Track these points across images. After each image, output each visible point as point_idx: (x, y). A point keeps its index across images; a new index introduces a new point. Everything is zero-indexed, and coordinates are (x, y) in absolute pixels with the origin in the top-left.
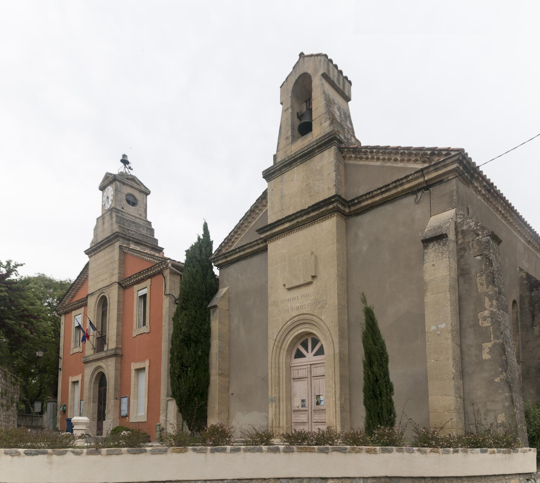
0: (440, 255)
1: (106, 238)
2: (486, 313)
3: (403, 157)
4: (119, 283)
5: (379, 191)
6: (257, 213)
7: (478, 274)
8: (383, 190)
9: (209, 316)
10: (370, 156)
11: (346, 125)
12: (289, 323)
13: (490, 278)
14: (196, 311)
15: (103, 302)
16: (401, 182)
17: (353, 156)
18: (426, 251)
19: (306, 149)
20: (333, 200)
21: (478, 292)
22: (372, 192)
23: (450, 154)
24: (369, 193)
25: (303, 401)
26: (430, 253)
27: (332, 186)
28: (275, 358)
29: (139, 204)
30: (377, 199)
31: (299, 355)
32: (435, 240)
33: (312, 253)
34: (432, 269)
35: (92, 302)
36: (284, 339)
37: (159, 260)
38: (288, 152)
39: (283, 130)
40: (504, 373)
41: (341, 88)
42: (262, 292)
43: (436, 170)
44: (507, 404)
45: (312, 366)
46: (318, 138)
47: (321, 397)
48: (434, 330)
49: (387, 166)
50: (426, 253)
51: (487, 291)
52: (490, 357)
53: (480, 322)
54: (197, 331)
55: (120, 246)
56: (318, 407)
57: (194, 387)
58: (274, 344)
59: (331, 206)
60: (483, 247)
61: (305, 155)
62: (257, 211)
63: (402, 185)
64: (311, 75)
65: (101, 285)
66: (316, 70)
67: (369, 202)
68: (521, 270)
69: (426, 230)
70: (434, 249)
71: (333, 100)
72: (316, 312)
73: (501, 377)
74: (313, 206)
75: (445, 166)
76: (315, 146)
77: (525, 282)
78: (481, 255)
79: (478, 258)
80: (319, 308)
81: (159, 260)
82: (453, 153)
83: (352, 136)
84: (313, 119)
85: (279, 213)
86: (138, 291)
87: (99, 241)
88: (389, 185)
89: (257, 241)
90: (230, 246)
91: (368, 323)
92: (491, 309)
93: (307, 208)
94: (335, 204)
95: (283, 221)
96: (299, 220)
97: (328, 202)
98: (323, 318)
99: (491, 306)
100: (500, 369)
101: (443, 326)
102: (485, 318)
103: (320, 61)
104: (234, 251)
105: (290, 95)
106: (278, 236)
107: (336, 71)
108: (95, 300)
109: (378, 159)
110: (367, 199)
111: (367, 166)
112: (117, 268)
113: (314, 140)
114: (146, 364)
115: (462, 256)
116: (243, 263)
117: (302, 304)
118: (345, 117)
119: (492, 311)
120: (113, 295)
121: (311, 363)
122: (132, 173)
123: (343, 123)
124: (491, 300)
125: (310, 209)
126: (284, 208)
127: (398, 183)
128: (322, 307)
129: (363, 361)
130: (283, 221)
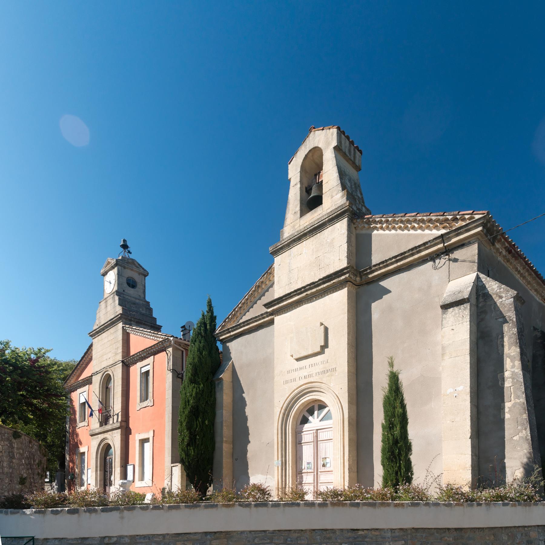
1: (110, 321)
4: (123, 361)
5: (394, 260)
9: (215, 388)
11: (357, 195)
12: (296, 391)
13: (512, 339)
15: (107, 380)
18: (445, 316)
23: (474, 218)
25: (308, 463)
29: (138, 286)
33: (322, 324)
35: (97, 380)
37: (162, 338)
38: (296, 227)
41: (352, 159)
42: (267, 364)
46: (329, 211)
48: (450, 393)
50: (445, 318)
55: (123, 327)
59: (343, 277)
64: (322, 148)
65: (105, 364)
66: (328, 144)
68: (535, 329)
69: (445, 296)
70: (453, 313)
71: (344, 171)
76: (327, 219)
77: (539, 341)
81: (162, 338)
83: (362, 206)
84: (324, 192)
86: (141, 368)
87: (102, 323)
88: (405, 253)
89: (262, 315)
91: (391, 387)
92: (513, 370)
93: (317, 280)
94: (347, 275)
99: (513, 366)
101: (460, 388)
103: (332, 134)
105: (299, 170)
107: (348, 142)
108: (99, 378)
112: (121, 348)
113: (325, 213)
114: (150, 435)
115: (482, 320)
118: (356, 187)
119: (513, 372)
120: (117, 374)
122: (132, 256)
123: (354, 193)
124: (512, 361)
126: (292, 282)
129: (383, 424)
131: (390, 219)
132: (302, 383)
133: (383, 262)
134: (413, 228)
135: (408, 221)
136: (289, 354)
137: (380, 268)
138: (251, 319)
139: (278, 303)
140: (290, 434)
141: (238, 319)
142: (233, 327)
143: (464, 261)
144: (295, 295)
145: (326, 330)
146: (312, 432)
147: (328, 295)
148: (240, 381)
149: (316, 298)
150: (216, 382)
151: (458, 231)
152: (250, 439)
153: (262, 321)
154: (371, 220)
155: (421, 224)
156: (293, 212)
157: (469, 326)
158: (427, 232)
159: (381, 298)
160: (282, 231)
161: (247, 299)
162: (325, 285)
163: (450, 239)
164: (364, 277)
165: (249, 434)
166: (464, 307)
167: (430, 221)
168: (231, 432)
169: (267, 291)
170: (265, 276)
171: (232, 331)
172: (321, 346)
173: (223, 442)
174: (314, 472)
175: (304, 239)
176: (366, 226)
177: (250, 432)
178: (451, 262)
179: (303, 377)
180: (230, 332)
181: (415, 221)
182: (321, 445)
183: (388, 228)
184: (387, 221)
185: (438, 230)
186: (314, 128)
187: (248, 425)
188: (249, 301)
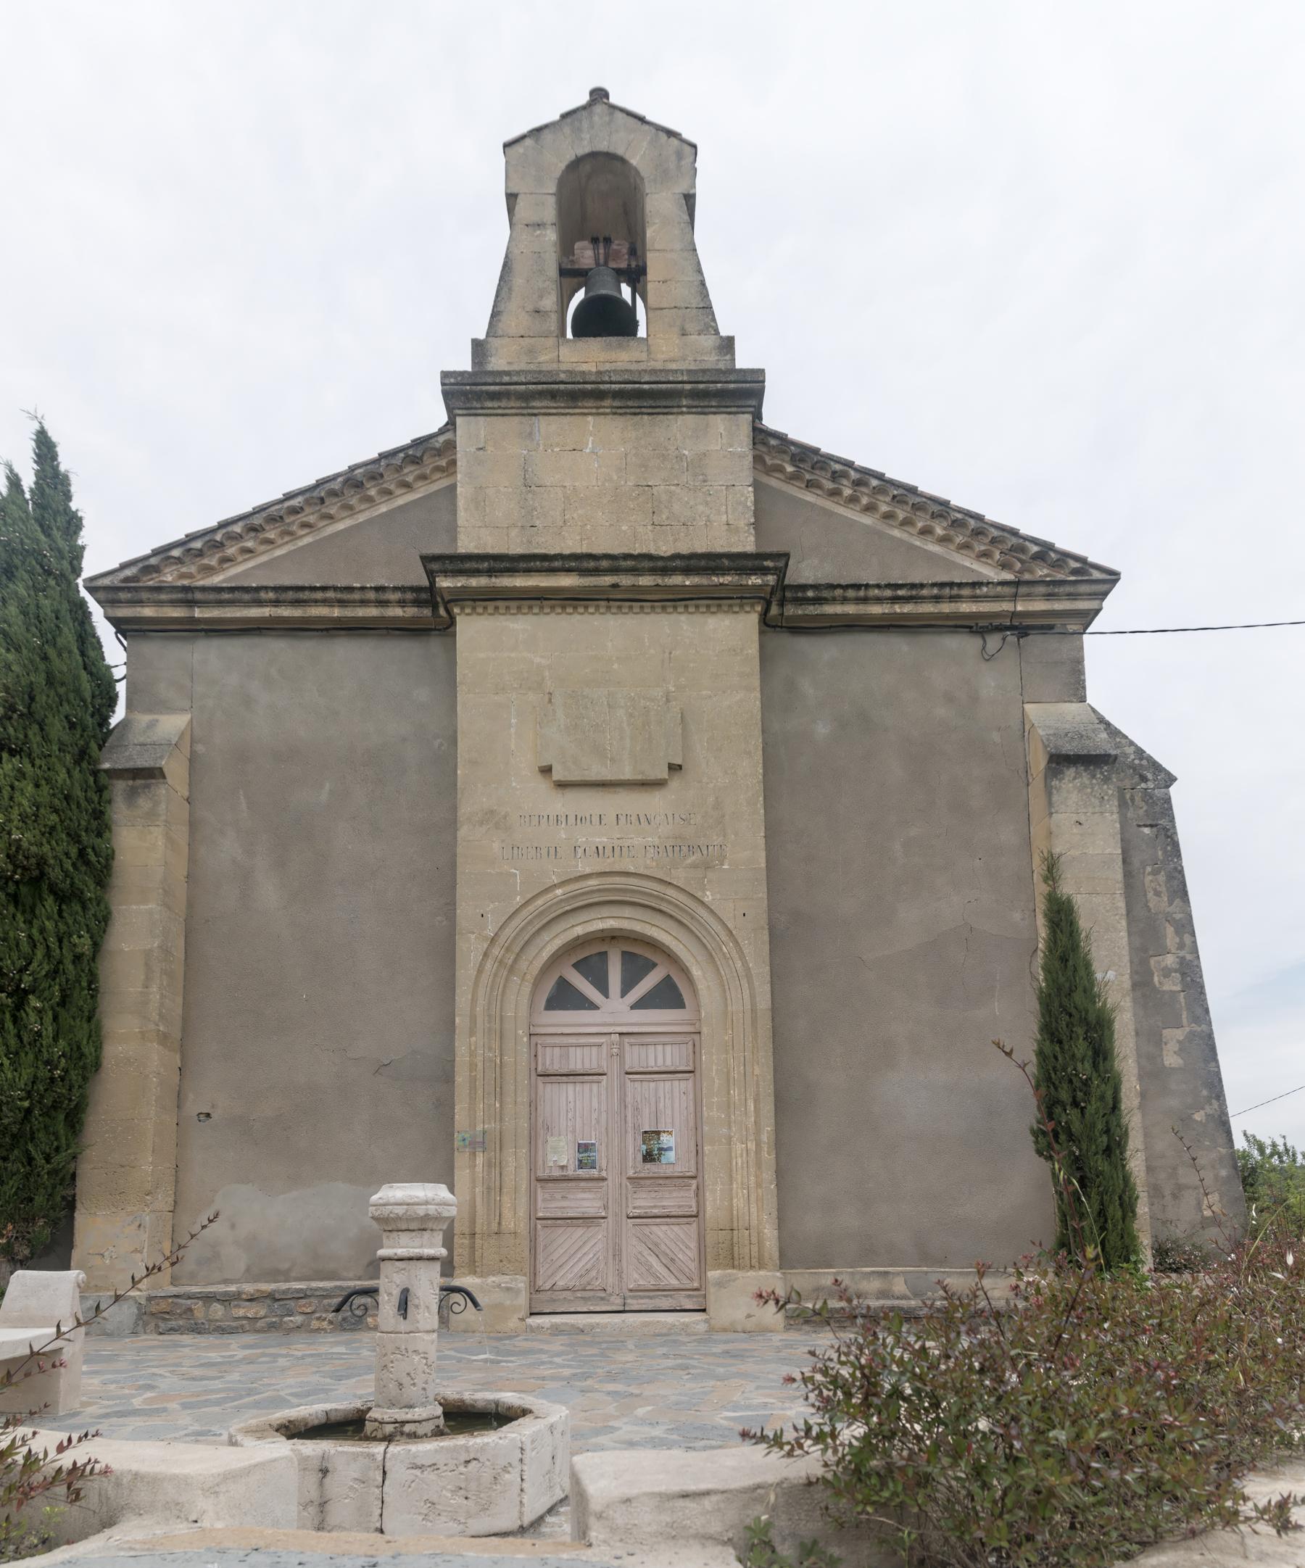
0: (1097, 802)
2: (1170, 960)
3: (952, 533)
5: (888, 593)
6: (370, 500)
7: (1149, 869)
8: (900, 593)
10: (847, 492)
14: (68, 772)
16: (955, 591)
17: (790, 469)
18: (1055, 783)
19: (647, 378)
20: (769, 563)
21: (1149, 910)
22: (867, 586)
24: (857, 587)
25: (584, 1148)
26: (1068, 792)
27: (742, 524)
28: (493, 1002)
30: (876, 609)
31: (564, 997)
32: (1083, 764)
36: (527, 943)
39: (518, 281)
40: (1214, 1101)
43: (1049, 596)
44: (1224, 1173)
47: (664, 1137)
49: (893, 538)
50: (1058, 790)
51: (1168, 909)
52: (1181, 1061)
53: (1156, 979)
54: (74, 851)
56: (651, 1168)
57: (52, 1080)
58: (486, 955)
59: (755, 580)
60: (1157, 809)
61: (640, 395)
62: (373, 492)
63: (954, 599)
67: (850, 609)
72: (679, 876)
73: (1208, 1109)
74: (693, 556)
75: (1072, 596)
76: (688, 387)
78: (1151, 826)
79: (1147, 830)
80: (694, 866)
82: (1097, 575)
85: (514, 533)
88: (922, 586)
90: (209, 570)
92: (1182, 953)
95: (557, 564)
96: (626, 580)
97: (750, 564)
98: (708, 897)
100: (1205, 1093)
102: (1167, 973)
104: (220, 595)
106: (513, 604)
109: (870, 508)
110: (845, 600)
111: (831, 514)
116: (278, 647)
117: (617, 843)
119: (1183, 958)
121: (624, 1030)
125: (678, 563)
127: (947, 591)
128: (707, 866)
130: (557, 564)
132: (588, 871)
136: (526, 764)
156: (530, 307)
166: (1102, 773)
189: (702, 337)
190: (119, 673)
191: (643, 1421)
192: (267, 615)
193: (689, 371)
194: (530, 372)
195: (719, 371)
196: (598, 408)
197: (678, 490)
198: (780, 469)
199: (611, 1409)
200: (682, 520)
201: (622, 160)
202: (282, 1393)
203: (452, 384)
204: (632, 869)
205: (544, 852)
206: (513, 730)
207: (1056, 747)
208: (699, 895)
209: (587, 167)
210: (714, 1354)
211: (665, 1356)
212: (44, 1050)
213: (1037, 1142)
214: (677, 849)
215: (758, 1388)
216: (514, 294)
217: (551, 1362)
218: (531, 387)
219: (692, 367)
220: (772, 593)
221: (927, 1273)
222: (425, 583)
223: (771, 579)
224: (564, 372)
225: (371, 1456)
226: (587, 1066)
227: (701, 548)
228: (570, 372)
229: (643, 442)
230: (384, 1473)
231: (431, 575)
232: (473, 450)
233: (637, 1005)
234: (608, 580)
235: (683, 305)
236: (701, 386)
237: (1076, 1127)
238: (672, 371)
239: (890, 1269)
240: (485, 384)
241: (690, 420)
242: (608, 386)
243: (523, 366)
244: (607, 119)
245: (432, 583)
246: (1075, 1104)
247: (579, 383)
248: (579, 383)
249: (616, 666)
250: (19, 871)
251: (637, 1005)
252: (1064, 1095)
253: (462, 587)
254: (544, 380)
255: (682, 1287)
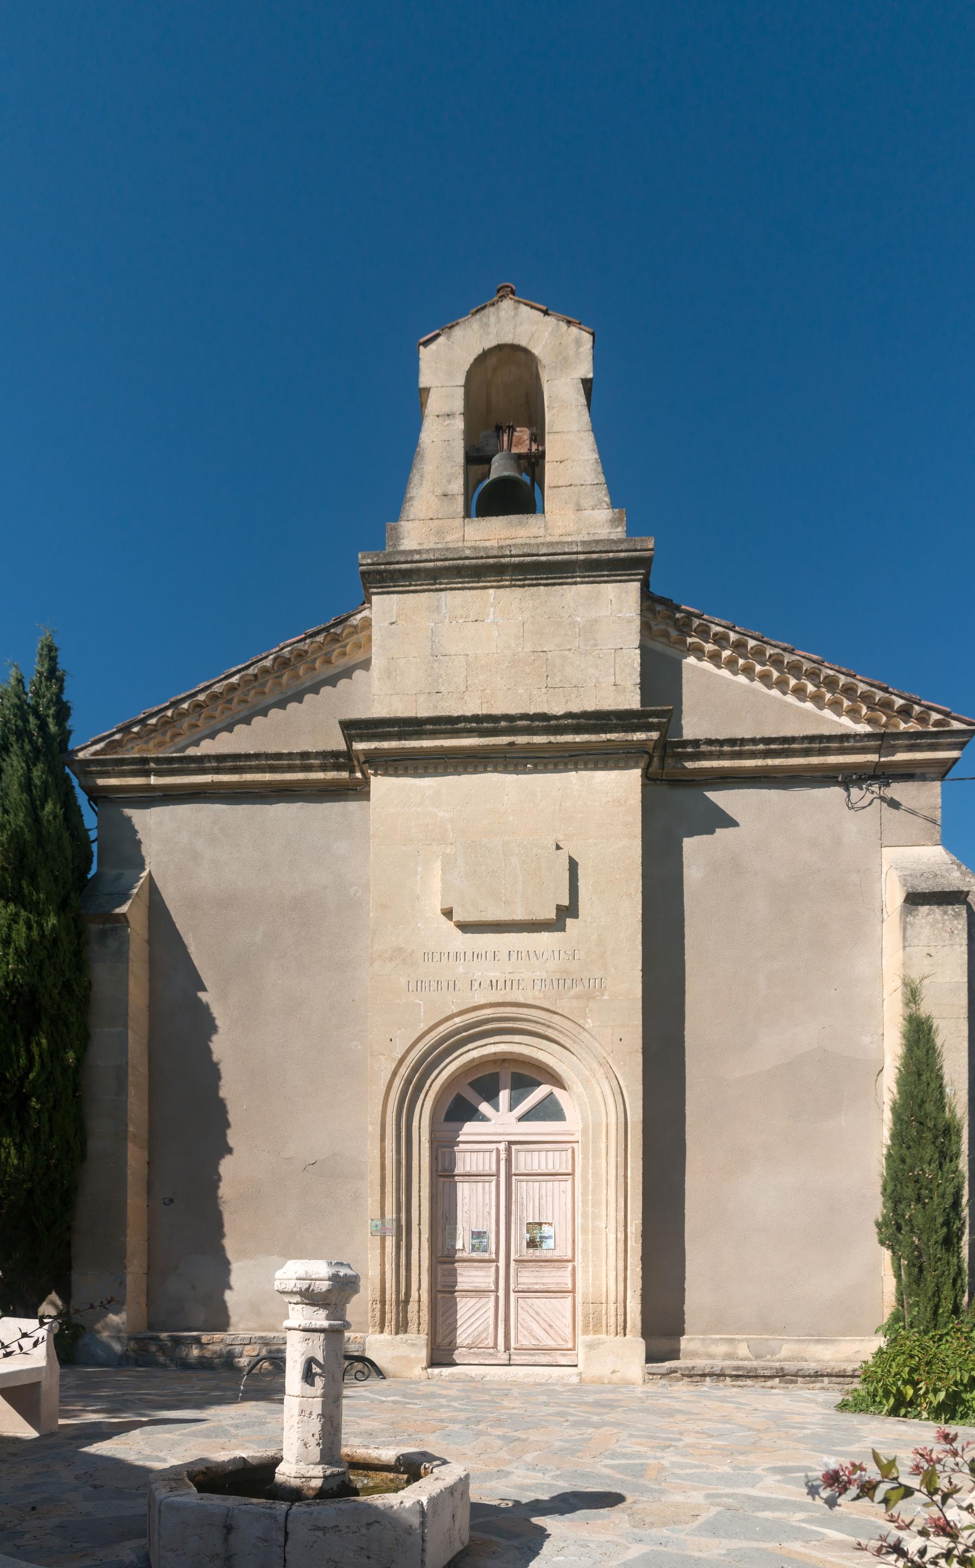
0: (947, 936)
5: (761, 747)
18: (910, 919)
23: (948, 724)
25: (478, 1235)
26: (921, 927)
34: (925, 962)
43: (911, 748)
45: (514, 1147)
47: (545, 1227)
59: (640, 736)
72: (563, 1006)
74: (585, 715)
76: (582, 557)
80: (577, 997)
85: (422, 698)
88: (793, 740)
98: (589, 1024)
117: (508, 977)
128: (590, 997)
131: (752, 643)
132: (483, 1001)
133: (732, 742)
134: (799, 692)
135: (795, 669)
136: (436, 905)
137: (721, 756)
138: (257, 756)
139: (400, 736)
140: (426, 1145)
141: (180, 741)
142: (170, 760)
143: (913, 812)
144: (469, 732)
145: (573, 866)
146: (494, 1146)
147: (576, 769)
148: (184, 947)
149: (535, 765)
150: (94, 928)
151: (914, 741)
152: (231, 1141)
153: (300, 776)
154: (696, 622)
155: (824, 690)
156: (439, 491)
157: (966, 956)
158: (828, 713)
159: (712, 832)
160: (394, 529)
161: (233, 688)
162: (578, 738)
163: (894, 750)
164: (670, 761)
165: (228, 1125)
166: (954, 910)
167: (849, 691)
168: (146, 1108)
169: (315, 689)
170: (320, 638)
171: (159, 773)
172: (559, 908)
173: (126, 1139)
174: (497, 1260)
175: (492, 580)
176: (674, 633)
177: (231, 1117)
178: (885, 805)
179: (486, 984)
180: (147, 773)
181: (813, 675)
182: (523, 1189)
183: (731, 664)
184: (739, 646)
185: (856, 720)
186: (513, 292)
187: (222, 1094)
188: (237, 695)
189: (596, 512)
190: (93, 835)
191: (533, 1467)
192: (210, 780)
193: (583, 543)
194: (438, 549)
195: (613, 542)
196: (499, 581)
197: (570, 654)
198: (666, 634)
199: (503, 1454)
200: (574, 682)
201: (525, 351)
202: (224, 1423)
203: (368, 565)
204: (522, 1000)
205: (445, 985)
206: (419, 877)
207: (912, 887)
208: (581, 1022)
209: (493, 361)
210: (586, 1403)
211: (546, 1404)
212: (42, 1143)
213: (880, 1233)
214: (561, 982)
215: (630, 1436)
216: (424, 482)
217: (449, 1406)
218: (439, 564)
219: (586, 538)
220: (654, 748)
221: (767, 1340)
222: (343, 747)
223: (655, 735)
224: (469, 548)
225: (273, 1517)
226: (481, 1168)
227: (590, 707)
228: (475, 548)
229: (539, 611)
230: (286, 1534)
231: (349, 739)
232: (387, 624)
233: (523, 1118)
234: (504, 740)
235: (578, 482)
236: (595, 556)
237: (919, 1220)
238: (567, 543)
239: (736, 1337)
240: (398, 563)
241: (583, 589)
242: (507, 560)
243: (432, 546)
244: (513, 313)
245: (349, 746)
246: (919, 1199)
247: (482, 558)
248: (482, 558)
249: (511, 818)
250: (15, 997)
251: (523, 1118)
252: (909, 1192)
253: (376, 749)
254: (451, 556)
255: (558, 1347)
